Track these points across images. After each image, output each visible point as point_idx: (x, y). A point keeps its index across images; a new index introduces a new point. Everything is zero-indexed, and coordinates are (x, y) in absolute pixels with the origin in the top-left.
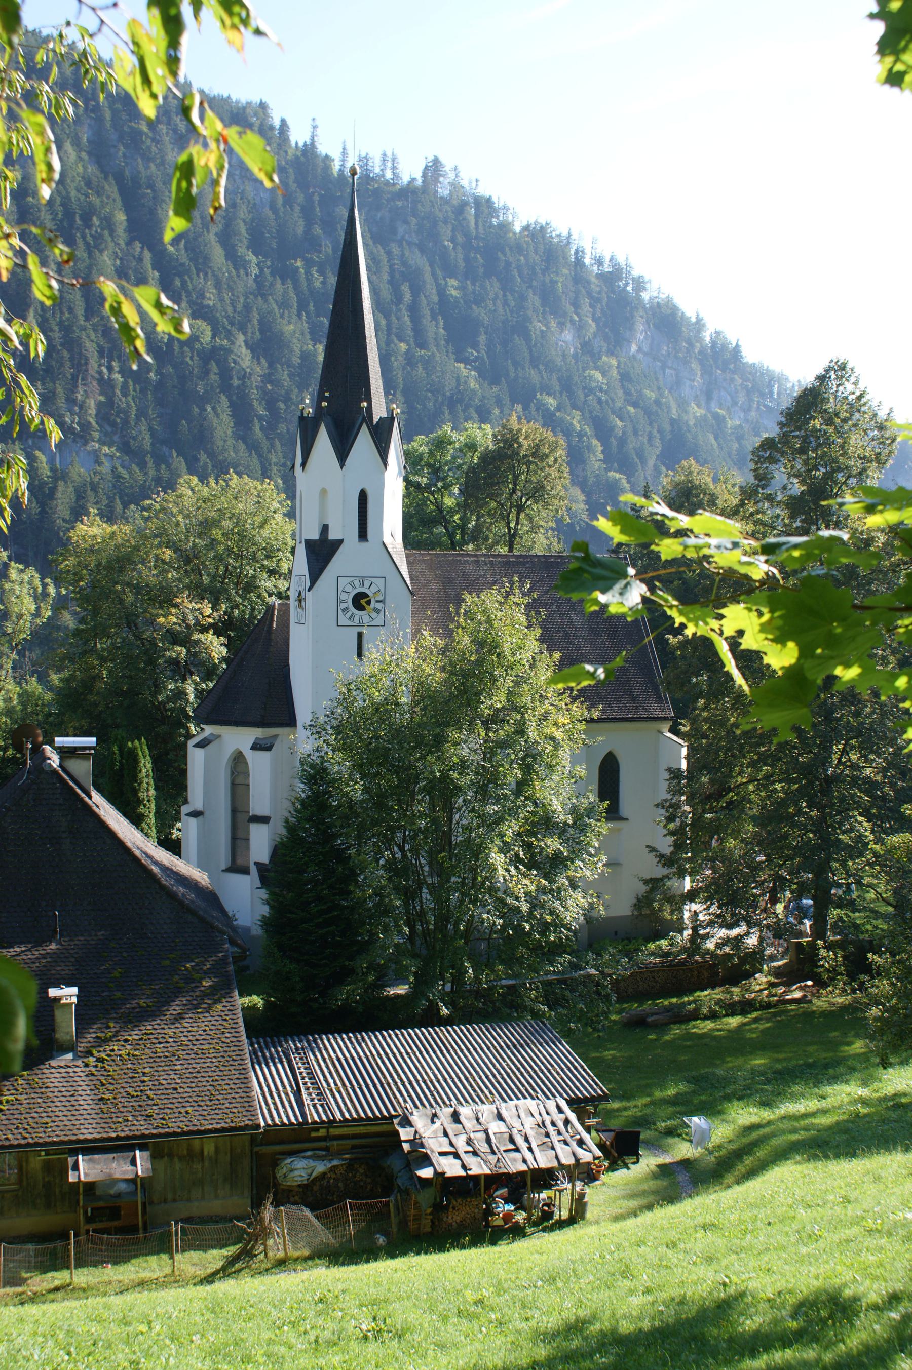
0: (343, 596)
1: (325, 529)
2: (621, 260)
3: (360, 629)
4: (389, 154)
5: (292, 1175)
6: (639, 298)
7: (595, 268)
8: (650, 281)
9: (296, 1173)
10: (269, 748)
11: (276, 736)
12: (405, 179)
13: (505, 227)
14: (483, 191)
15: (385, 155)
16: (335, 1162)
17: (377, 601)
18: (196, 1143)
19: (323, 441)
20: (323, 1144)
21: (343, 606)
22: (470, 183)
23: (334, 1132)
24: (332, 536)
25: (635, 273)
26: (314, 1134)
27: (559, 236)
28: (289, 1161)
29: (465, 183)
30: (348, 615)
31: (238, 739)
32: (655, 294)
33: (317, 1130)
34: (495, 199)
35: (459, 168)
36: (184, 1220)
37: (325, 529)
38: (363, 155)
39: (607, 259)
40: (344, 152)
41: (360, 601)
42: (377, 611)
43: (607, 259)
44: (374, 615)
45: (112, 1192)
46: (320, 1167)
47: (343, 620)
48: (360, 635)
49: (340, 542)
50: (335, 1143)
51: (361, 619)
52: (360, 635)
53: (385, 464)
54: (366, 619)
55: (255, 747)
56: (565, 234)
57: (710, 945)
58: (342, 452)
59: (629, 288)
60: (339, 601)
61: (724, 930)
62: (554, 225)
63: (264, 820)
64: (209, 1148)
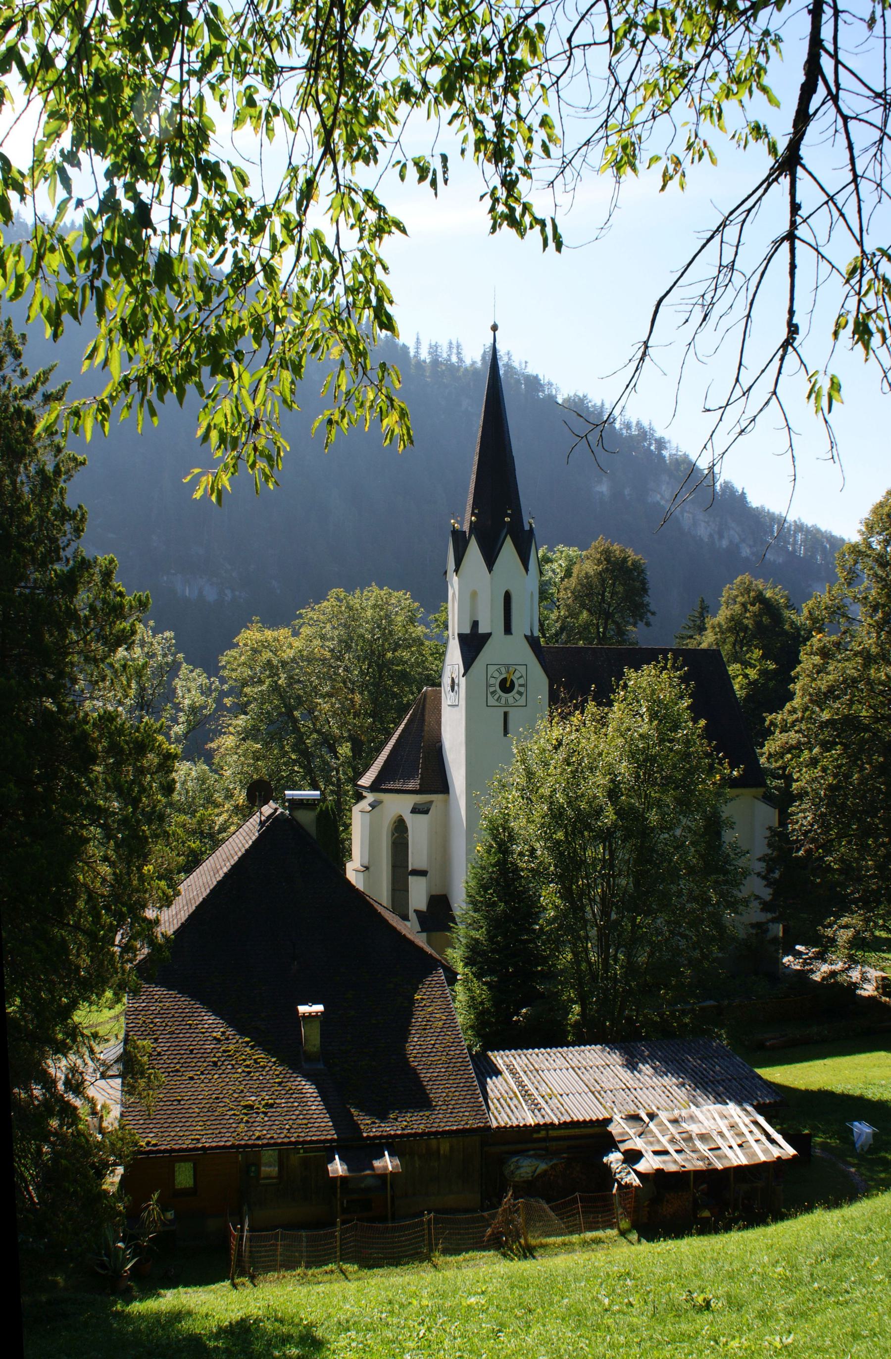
0: (492, 681)
1: (475, 624)
2: (646, 424)
3: (506, 709)
4: (454, 343)
5: (518, 1172)
6: (660, 454)
7: (624, 431)
8: (669, 442)
9: (522, 1170)
10: (426, 812)
11: (431, 802)
12: (468, 362)
13: (552, 399)
14: (531, 370)
15: (451, 343)
16: (555, 1161)
17: (520, 685)
18: (434, 1143)
19: (474, 550)
20: (543, 1145)
21: (492, 689)
22: (520, 364)
23: (553, 1133)
24: (482, 630)
25: (658, 435)
26: (535, 1136)
27: (594, 406)
28: (515, 1159)
29: (516, 364)
30: (496, 697)
31: (398, 805)
32: (674, 452)
33: (538, 1132)
34: (541, 377)
35: (512, 353)
36: (437, 1211)
37: (475, 624)
38: (433, 343)
39: (634, 424)
40: (418, 342)
41: (506, 686)
42: (520, 693)
43: (634, 424)
44: (517, 697)
45: (363, 1186)
46: (543, 1167)
47: (492, 701)
48: (506, 714)
49: (489, 635)
50: (554, 1143)
51: (507, 700)
52: (506, 714)
53: (527, 570)
54: (511, 701)
55: (415, 810)
56: (599, 404)
57: (817, 977)
58: (490, 560)
59: (653, 448)
60: (488, 686)
61: (63, 1077)
62: (589, 397)
63: (423, 873)
64: (445, 1147)
